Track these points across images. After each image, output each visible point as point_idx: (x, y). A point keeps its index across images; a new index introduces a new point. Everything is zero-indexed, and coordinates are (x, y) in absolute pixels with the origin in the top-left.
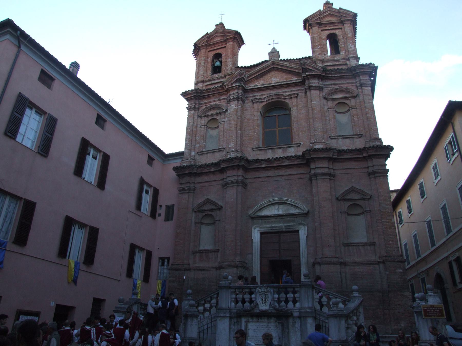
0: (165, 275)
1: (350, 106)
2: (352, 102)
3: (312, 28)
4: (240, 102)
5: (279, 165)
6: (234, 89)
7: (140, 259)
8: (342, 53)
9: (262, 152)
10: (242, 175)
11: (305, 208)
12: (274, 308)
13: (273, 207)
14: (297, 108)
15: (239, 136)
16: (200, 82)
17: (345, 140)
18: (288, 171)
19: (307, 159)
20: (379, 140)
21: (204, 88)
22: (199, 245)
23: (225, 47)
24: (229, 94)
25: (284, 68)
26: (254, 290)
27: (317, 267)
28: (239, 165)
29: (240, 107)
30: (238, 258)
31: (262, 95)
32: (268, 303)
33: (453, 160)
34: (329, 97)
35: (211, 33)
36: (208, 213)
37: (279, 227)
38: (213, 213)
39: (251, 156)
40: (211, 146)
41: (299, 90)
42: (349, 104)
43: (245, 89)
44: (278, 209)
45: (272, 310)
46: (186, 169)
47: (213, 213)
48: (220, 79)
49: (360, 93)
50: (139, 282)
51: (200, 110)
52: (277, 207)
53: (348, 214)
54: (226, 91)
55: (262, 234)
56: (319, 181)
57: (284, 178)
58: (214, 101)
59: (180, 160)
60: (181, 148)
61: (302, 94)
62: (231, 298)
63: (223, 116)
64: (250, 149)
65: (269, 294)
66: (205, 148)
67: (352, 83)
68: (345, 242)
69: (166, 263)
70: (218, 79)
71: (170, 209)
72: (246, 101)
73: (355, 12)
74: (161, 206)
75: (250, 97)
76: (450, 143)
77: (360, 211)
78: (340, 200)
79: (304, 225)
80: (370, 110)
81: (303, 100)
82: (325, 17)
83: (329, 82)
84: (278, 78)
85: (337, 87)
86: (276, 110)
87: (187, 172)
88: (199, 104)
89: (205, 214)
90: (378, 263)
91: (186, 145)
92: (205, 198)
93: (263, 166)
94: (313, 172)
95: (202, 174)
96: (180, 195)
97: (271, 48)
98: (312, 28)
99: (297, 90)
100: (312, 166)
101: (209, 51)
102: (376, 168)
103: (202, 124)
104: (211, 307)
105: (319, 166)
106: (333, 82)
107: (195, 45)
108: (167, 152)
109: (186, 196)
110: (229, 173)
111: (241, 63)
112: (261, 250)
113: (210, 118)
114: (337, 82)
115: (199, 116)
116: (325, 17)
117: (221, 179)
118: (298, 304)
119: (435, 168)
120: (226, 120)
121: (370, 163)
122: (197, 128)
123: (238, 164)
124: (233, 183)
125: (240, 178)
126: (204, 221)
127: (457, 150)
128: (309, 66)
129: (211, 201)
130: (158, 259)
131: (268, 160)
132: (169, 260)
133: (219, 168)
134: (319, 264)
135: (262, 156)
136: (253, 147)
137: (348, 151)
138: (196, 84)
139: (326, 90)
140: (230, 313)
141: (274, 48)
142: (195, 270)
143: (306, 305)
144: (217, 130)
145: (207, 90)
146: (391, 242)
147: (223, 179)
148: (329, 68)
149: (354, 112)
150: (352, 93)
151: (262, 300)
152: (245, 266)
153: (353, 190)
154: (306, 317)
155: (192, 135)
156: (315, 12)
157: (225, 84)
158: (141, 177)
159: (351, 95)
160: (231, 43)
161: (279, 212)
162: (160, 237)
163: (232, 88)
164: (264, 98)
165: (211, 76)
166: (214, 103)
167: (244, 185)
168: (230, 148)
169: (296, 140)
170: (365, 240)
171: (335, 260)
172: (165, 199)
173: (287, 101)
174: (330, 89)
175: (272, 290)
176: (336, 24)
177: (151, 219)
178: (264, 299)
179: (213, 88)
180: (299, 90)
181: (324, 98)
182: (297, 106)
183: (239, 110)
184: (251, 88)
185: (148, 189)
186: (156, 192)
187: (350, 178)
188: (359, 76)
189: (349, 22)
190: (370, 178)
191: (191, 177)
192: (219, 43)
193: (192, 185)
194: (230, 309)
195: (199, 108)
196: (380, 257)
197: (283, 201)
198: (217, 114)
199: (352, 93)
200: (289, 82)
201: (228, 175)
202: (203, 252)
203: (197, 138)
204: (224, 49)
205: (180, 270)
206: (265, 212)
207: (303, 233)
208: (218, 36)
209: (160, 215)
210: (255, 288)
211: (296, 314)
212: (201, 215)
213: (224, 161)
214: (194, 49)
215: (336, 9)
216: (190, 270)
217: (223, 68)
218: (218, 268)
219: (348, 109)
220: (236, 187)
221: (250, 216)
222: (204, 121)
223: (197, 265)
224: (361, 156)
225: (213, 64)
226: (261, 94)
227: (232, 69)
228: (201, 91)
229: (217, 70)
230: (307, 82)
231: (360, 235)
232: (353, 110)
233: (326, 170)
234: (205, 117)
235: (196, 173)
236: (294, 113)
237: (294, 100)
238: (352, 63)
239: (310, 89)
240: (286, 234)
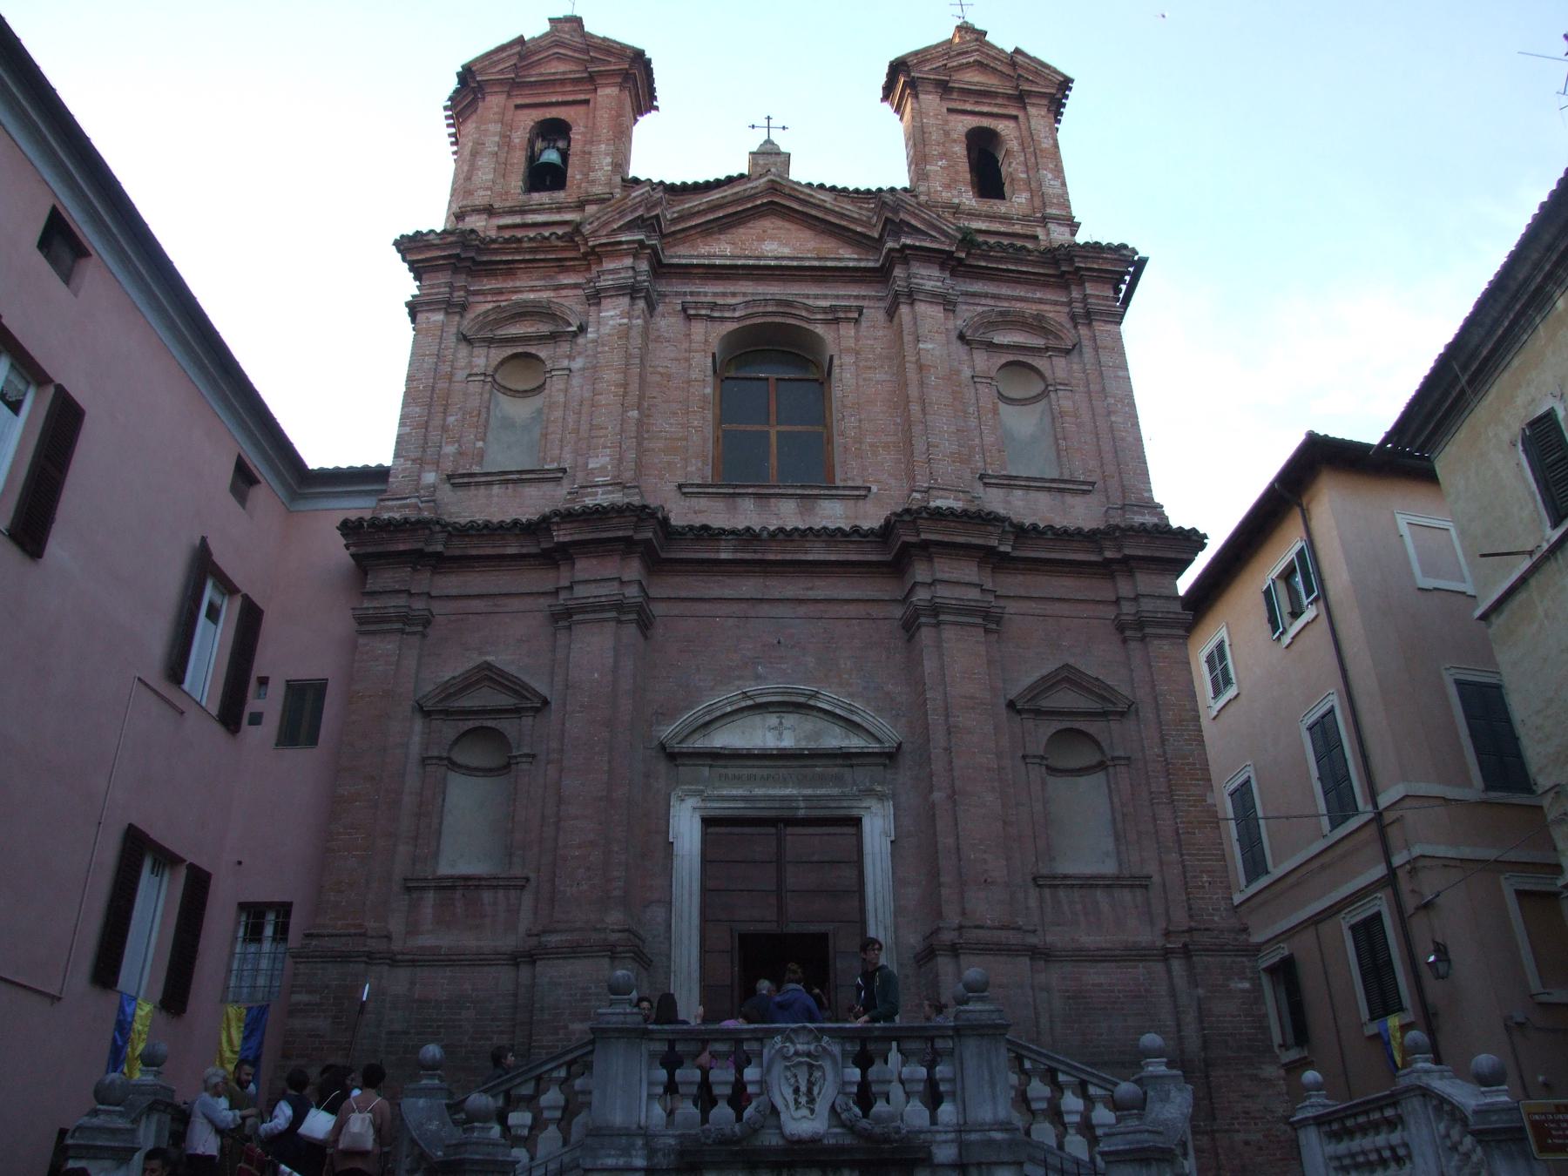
0: (261, 981)
1: (1050, 381)
2: (1058, 368)
3: (916, 96)
4: (641, 304)
5: (789, 557)
7: (155, 904)
9: (719, 504)
10: (640, 583)
11: (889, 732)
12: (850, 1127)
13: (757, 719)
14: (857, 357)
15: (632, 429)
16: (477, 211)
17: (1033, 494)
18: (823, 588)
19: (899, 546)
20: (1157, 509)
21: (493, 234)
22: (436, 855)
23: (587, 102)
24: (595, 269)
25: (813, 212)
26: (755, 1046)
27: (944, 964)
28: (628, 541)
29: (639, 321)
30: (615, 917)
31: (724, 295)
32: (822, 1106)
33: (1293, 631)
35: (533, 39)
36: (486, 723)
37: (783, 798)
38: (506, 725)
39: (681, 513)
40: (503, 457)
41: (864, 297)
42: (1048, 373)
43: (659, 261)
44: (779, 730)
45: (836, 1137)
46: (395, 540)
47: (506, 725)
48: (559, 210)
49: (1085, 342)
50: (144, 1011)
51: (470, 315)
52: (773, 720)
53: (1052, 770)
54: (585, 256)
55: (707, 822)
56: (949, 633)
57: (802, 610)
58: (532, 289)
59: (370, 502)
60: (382, 455)
61: (875, 314)
62: (651, 1084)
63: (565, 347)
64: (673, 486)
65: (827, 1065)
66: (480, 464)
67: (1056, 303)
68: (1044, 871)
69: (269, 931)
70: (550, 210)
71: (305, 700)
72: (660, 308)
73: (1070, 74)
74: (263, 681)
75: (677, 294)
76: (1287, 575)
77: (1088, 757)
78: (1019, 712)
79: (882, 798)
80: (1121, 401)
81: (880, 333)
82: (961, 67)
83: (978, 287)
84: (786, 245)
86: (773, 358)
87: (402, 547)
89: (470, 724)
90: (1166, 955)
91: (401, 441)
92: (476, 660)
93: (723, 556)
94: (922, 595)
95: (464, 562)
96: (362, 640)
97: (755, 141)
98: (916, 96)
99: (857, 297)
100: (921, 572)
101: (518, 107)
102: (1147, 605)
103: (476, 370)
104: (538, 1125)
105: (946, 576)
106: (991, 288)
107: (467, 75)
108: (313, 463)
109: (386, 646)
110: (585, 567)
111: (639, 167)
112: (707, 892)
113: (510, 351)
114: (1005, 290)
115: (465, 339)
116: (961, 67)
117: (550, 587)
118: (947, 1111)
119: (1217, 658)
120: (577, 364)
121: (1124, 588)
122: (450, 381)
123: (630, 533)
124: (602, 608)
125: (632, 592)
126: (460, 757)
127: (1316, 599)
128: (915, 216)
129: (502, 673)
130: (234, 909)
131: (748, 537)
132: (288, 914)
133: (544, 545)
134: (954, 950)
135: (717, 515)
136: (682, 481)
137: (1049, 535)
138: (459, 216)
139: (967, 313)
140: (651, 1152)
141: (768, 142)
143: (985, 1112)
144: (537, 402)
145: (507, 241)
147: (556, 592)
148: (980, 239)
149: (1064, 401)
150: (1057, 337)
151: (797, 1091)
152: (641, 952)
153: (1068, 677)
154: (990, 1164)
155: (430, 405)
156: (934, 42)
157: (587, 229)
158: (204, 539)
159: (1052, 343)
160: (612, 91)
162: (252, 813)
163: (613, 250)
164: (733, 308)
165: (523, 198)
166: (532, 296)
167: (645, 624)
169: (848, 471)
170: (1109, 868)
171: (1013, 938)
172: (284, 657)
173: (819, 329)
174: (980, 309)
175: (836, 1049)
176: (999, 101)
177: (218, 729)
178: (803, 1089)
179: (531, 239)
180: (864, 297)
181: (961, 337)
182: (857, 353)
183: (633, 333)
184: (684, 261)
185: (218, 600)
186: (251, 618)
187: (1057, 631)
188: (1081, 283)
189: (1045, 102)
190: (1125, 641)
191: (414, 570)
192: (562, 82)
193: (419, 605)
194: (645, 1133)
195: (463, 308)
196: (1167, 934)
197: (802, 700)
198: (541, 339)
199: (1057, 337)
200: (829, 264)
201: (579, 576)
202: (453, 888)
203: (451, 419)
204: (582, 109)
205: (344, 958)
206: (724, 739)
207: (877, 828)
209: (256, 719)
210: (760, 1040)
212: (450, 730)
213: (568, 516)
214: (457, 91)
215: (1002, 51)
216: (393, 961)
217: (574, 174)
218: (516, 959)
219: (1041, 387)
220: (613, 624)
221: (663, 747)
222: (483, 359)
223: (425, 941)
224: (1093, 558)
225: (532, 158)
226: (720, 289)
227: (609, 183)
228: (482, 240)
229: (544, 177)
230: (898, 272)
231: (1087, 849)
232: (1060, 393)
233: (973, 594)
234: (490, 342)
235: (438, 555)
236: (846, 379)
237: (847, 331)
238: (1054, 236)
239: (911, 296)
240: (811, 830)
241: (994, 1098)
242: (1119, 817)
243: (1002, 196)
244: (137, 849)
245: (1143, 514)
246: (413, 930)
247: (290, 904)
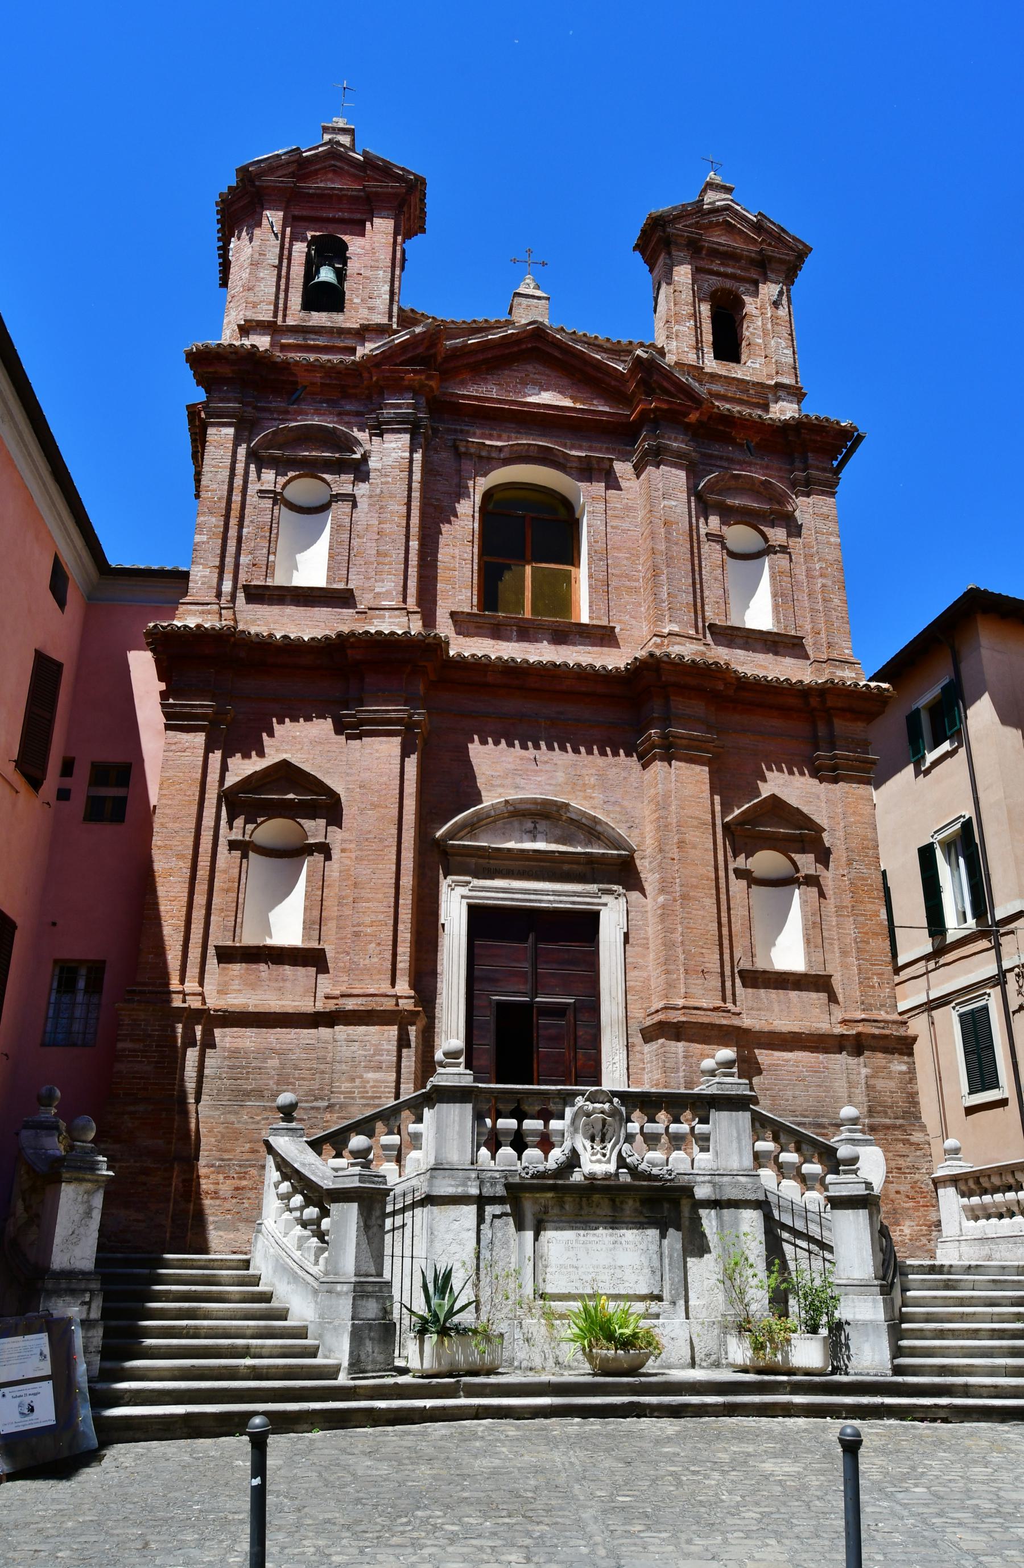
69: (81, 984)
165: (303, 314)
243: (737, 360)
245: (844, 670)
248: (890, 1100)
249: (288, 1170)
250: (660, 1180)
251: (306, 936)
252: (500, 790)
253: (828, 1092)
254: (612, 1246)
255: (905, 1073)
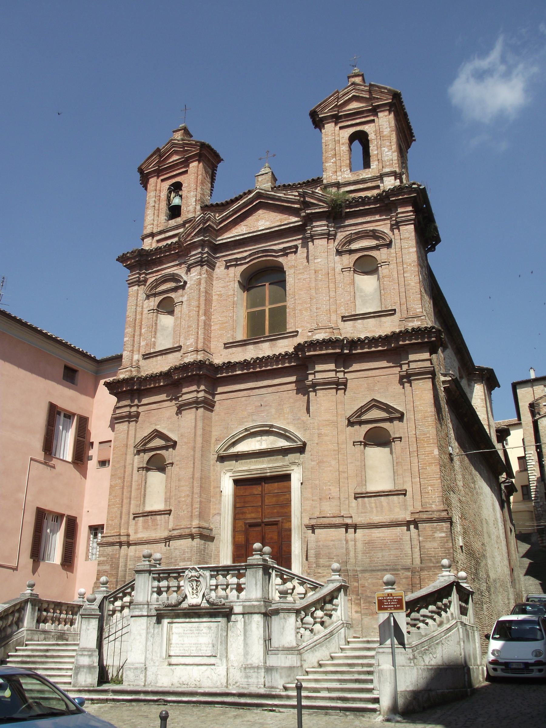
2: (381, 255)
6: (196, 248)
8: (374, 165)
30: (195, 523)
34: (346, 248)
37: (261, 469)
40: (164, 342)
51: (148, 284)
55: (237, 482)
72: (217, 265)
85: (360, 228)
88: (147, 274)
118: (243, 594)
131: (245, 364)
139: (340, 236)
140: (149, 610)
142: (135, 544)
146: (430, 488)
151: (193, 589)
152: (206, 536)
159: (381, 242)
161: (261, 445)
163: (194, 246)
168: (188, 347)
169: (290, 327)
170: (387, 486)
171: (338, 521)
173: (280, 259)
174: (348, 233)
183: (203, 282)
206: (241, 448)
208: (176, 152)
211: (237, 609)
213: (176, 369)
216: (129, 544)
217: (184, 209)
218: (168, 540)
237: (291, 257)
239: (312, 238)
241: (256, 584)
242: (395, 463)
244: (41, 515)
245: (413, 321)
246: (136, 532)
247: (104, 525)
248: (433, 553)
249: (328, 598)
250: (217, 605)
251: (166, 505)
252: (246, 424)
253: (402, 551)
254: (197, 635)
255: (444, 537)
